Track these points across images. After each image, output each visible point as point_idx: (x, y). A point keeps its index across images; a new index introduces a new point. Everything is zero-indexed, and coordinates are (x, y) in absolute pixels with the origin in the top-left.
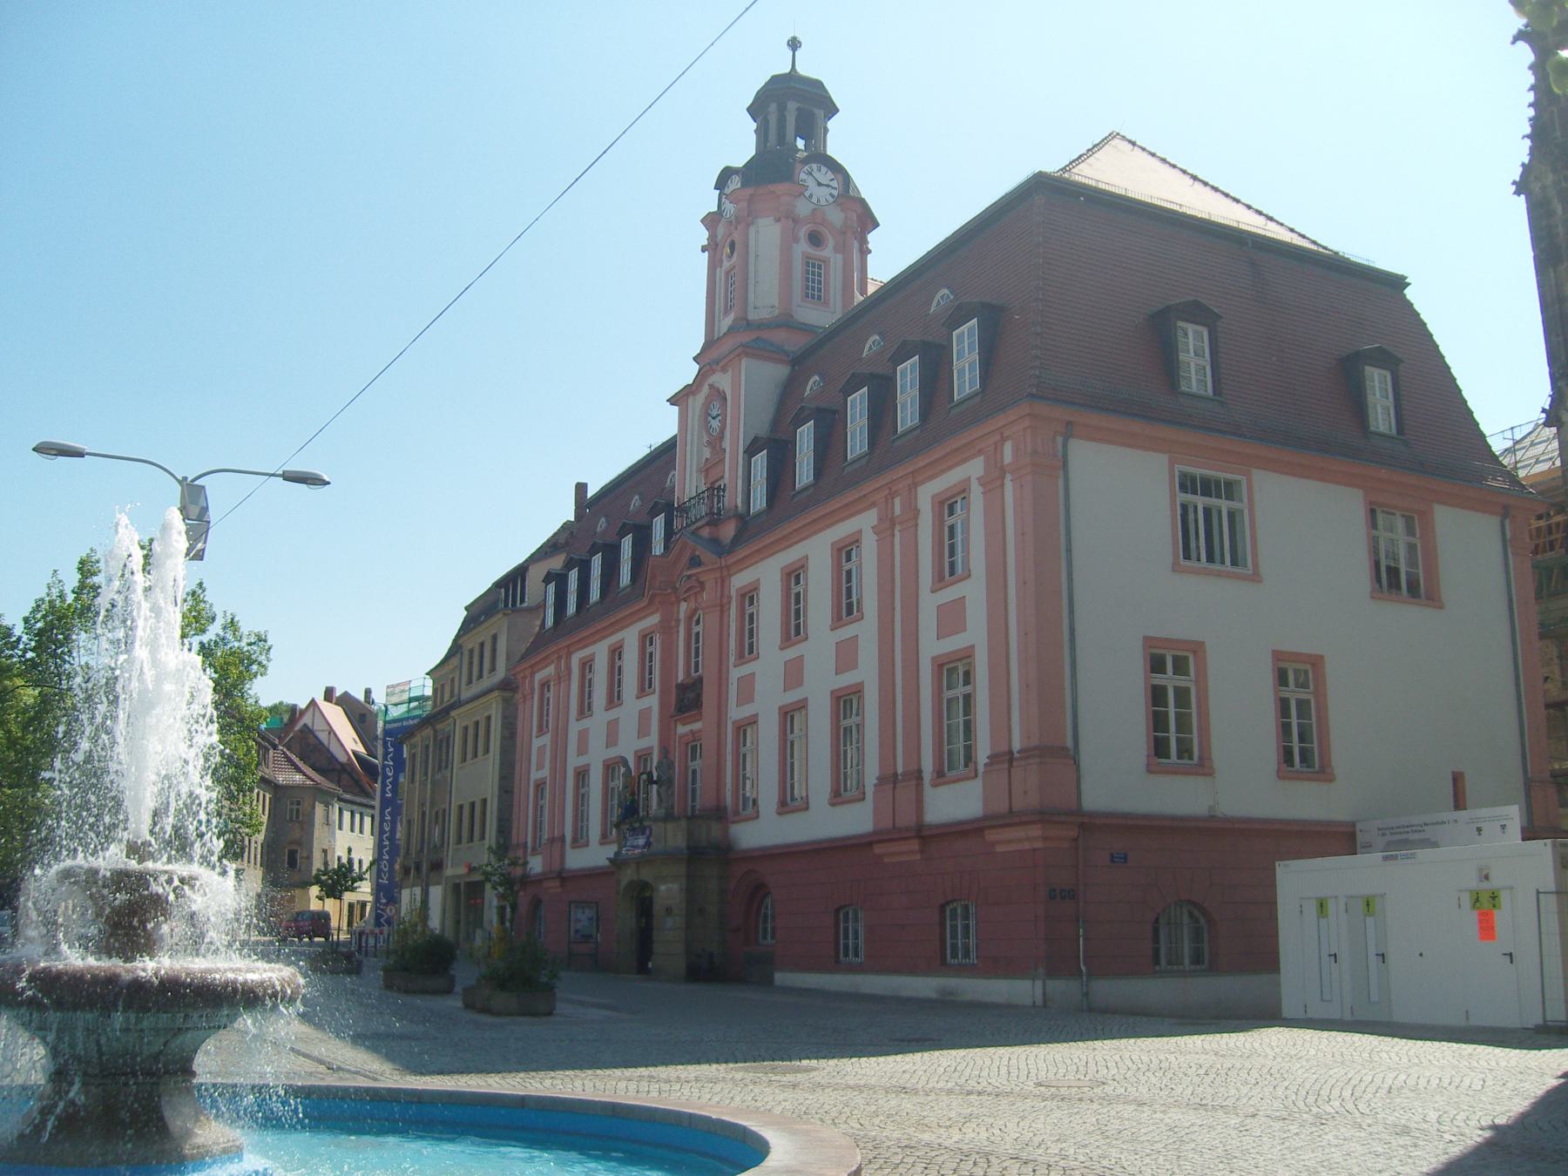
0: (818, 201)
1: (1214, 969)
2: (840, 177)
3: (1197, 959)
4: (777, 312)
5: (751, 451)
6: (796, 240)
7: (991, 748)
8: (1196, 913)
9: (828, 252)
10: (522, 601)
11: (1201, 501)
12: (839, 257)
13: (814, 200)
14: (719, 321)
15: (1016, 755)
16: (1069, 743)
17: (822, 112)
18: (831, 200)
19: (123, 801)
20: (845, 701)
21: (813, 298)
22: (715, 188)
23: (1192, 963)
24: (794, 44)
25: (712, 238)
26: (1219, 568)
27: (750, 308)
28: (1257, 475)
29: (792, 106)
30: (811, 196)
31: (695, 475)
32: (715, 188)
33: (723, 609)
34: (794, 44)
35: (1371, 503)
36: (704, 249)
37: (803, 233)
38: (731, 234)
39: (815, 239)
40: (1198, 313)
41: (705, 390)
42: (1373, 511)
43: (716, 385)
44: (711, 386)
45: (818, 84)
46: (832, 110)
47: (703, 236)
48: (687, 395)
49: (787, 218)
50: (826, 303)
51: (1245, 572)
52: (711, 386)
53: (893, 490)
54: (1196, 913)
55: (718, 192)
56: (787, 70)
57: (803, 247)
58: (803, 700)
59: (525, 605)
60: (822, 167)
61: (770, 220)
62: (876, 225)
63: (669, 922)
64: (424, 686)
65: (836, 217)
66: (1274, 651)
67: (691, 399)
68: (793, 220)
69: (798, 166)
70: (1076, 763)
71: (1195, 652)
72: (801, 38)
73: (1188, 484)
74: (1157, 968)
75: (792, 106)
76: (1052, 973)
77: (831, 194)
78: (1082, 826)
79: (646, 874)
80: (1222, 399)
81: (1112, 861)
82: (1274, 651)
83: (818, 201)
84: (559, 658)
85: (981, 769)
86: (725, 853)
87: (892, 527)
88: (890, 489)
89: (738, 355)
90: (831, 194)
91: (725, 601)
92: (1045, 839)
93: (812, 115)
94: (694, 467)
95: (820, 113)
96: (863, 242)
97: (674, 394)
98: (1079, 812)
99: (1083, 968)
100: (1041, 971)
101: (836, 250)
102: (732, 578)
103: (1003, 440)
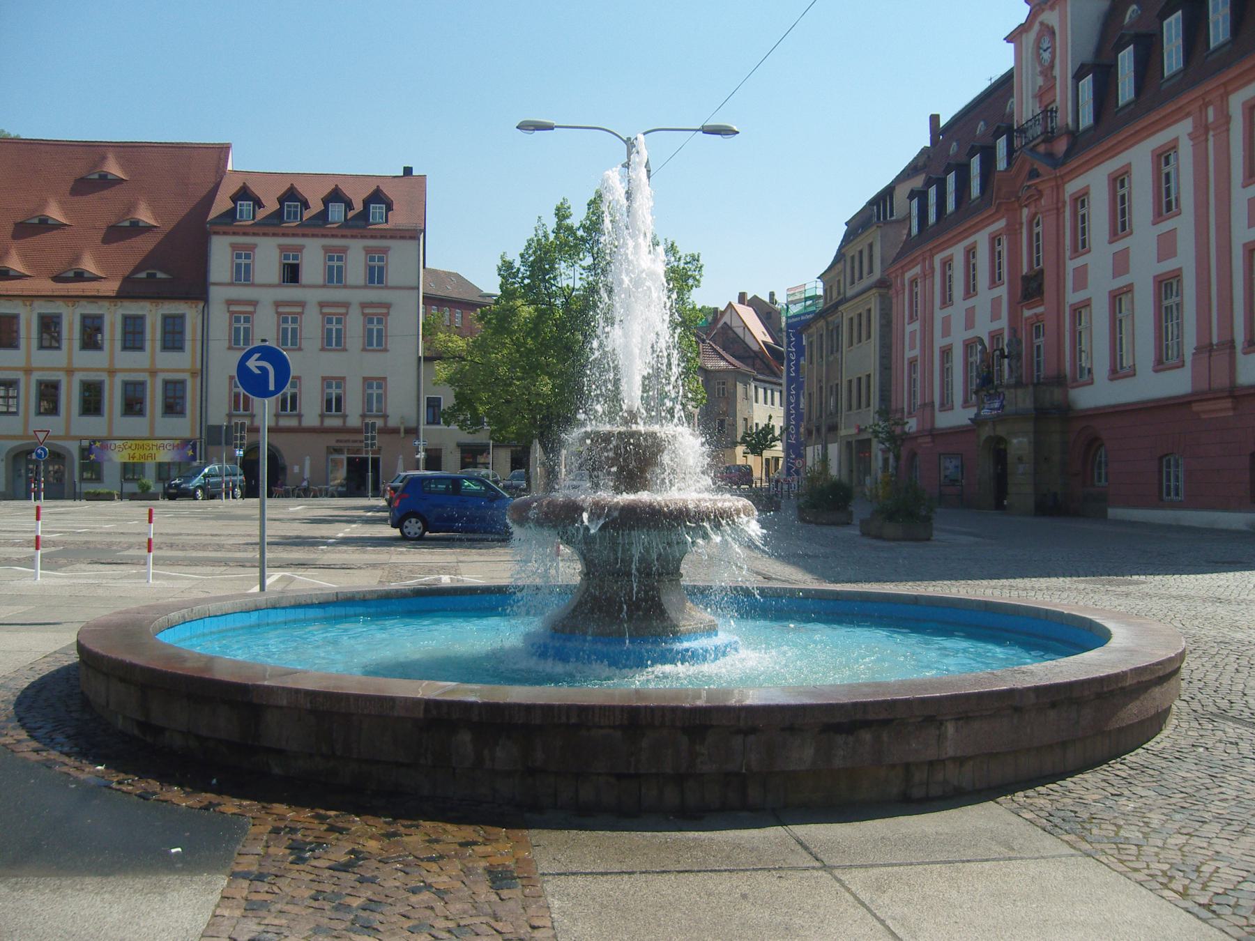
5: (1078, 76)
10: (892, 215)
33: (1059, 211)
41: (1036, 27)
52: (1042, 24)
59: (894, 218)
84: (924, 260)
86: (1066, 412)
87: (1207, 132)
88: (1204, 99)
94: (1030, 93)
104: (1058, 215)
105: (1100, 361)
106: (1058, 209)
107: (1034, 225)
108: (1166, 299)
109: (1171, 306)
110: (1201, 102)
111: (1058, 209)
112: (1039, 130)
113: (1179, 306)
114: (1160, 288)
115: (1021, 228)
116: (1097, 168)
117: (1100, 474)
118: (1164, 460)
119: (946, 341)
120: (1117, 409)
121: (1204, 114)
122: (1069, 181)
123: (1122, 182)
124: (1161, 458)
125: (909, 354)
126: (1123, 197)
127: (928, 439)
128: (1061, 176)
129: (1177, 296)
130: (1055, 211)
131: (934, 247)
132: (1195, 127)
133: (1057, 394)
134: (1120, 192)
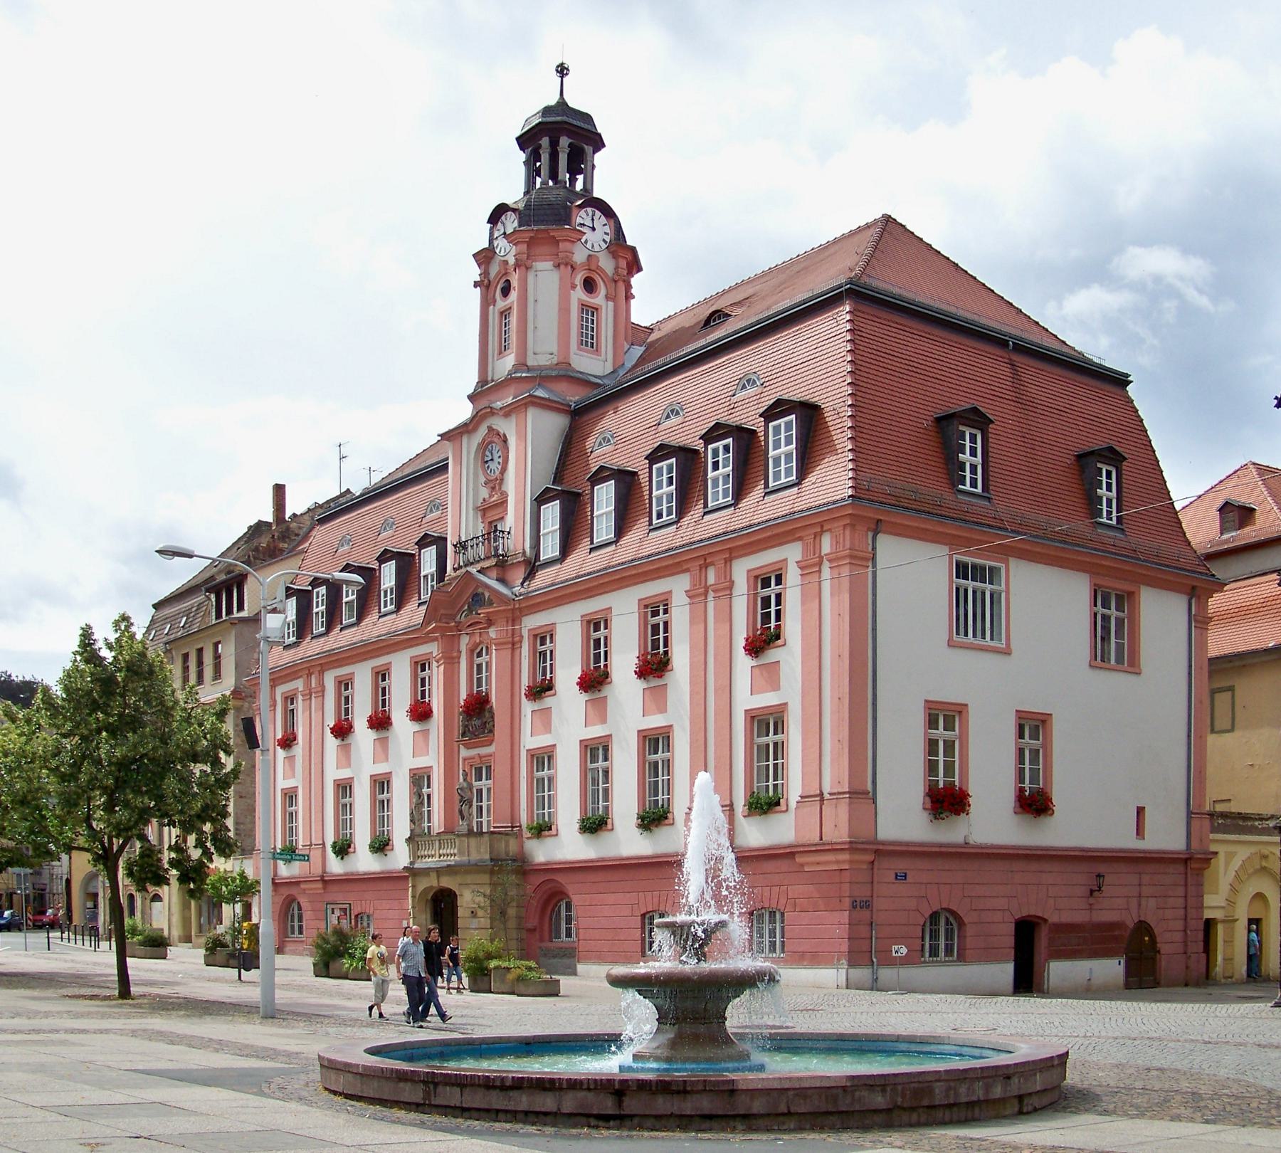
0: (593, 246)
1: (962, 958)
2: (612, 221)
3: (949, 950)
4: (555, 361)
5: (542, 499)
6: (574, 287)
7: (803, 789)
8: (951, 919)
9: (599, 299)
10: (241, 608)
11: (970, 585)
12: (611, 304)
13: (589, 246)
14: (493, 361)
15: (826, 796)
16: (869, 787)
17: (591, 149)
18: (604, 246)
19: (689, 880)
20: (382, 675)
21: (587, 345)
22: (488, 222)
23: (946, 956)
24: (562, 70)
25: (485, 274)
26: (980, 643)
27: (530, 353)
28: (1013, 562)
29: (564, 142)
30: (586, 241)
31: (471, 512)
32: (488, 222)
33: (514, 645)
34: (562, 70)
35: (1095, 585)
36: (476, 284)
37: (579, 280)
38: (506, 274)
39: (589, 285)
40: (978, 419)
41: (483, 431)
42: (1095, 591)
43: (494, 427)
44: (490, 429)
45: (587, 118)
46: (598, 143)
47: (475, 272)
48: (461, 434)
49: (566, 264)
50: (598, 351)
51: (1000, 645)
52: (490, 429)
53: (707, 561)
54: (951, 919)
55: (489, 225)
56: (553, 100)
57: (579, 294)
58: (351, 674)
59: (244, 614)
60: (597, 211)
61: (548, 265)
62: (639, 269)
63: (474, 923)
64: (1140, 885)
65: (607, 264)
66: (1017, 711)
67: (465, 439)
68: (572, 267)
69: (575, 211)
70: (874, 802)
71: (960, 712)
72: (568, 63)
73: (962, 570)
74: (923, 959)
75: (564, 142)
76: (852, 964)
77: (604, 240)
78: (877, 852)
79: (447, 882)
80: (989, 496)
81: (896, 878)
82: (1017, 711)
83: (593, 246)
84: (310, 675)
85: (793, 804)
86: (523, 867)
87: (706, 594)
88: (705, 560)
89: (525, 404)
90: (604, 240)
91: (517, 639)
92: (851, 862)
93: (582, 150)
94: (471, 506)
95: (588, 149)
96: (628, 287)
97: (447, 430)
98: (875, 842)
99: (874, 960)
100: (844, 961)
101: (607, 298)
102: (524, 619)
103: (822, 532)
104: (513, 649)
105: (568, 811)
106: (513, 644)
107: (475, 655)
108: (537, 771)
109: (543, 779)
110: (702, 562)
111: (513, 644)
112: (481, 550)
113: (668, 763)
114: (532, 763)
115: (459, 657)
116: (583, 601)
117: (293, 927)
118: (647, 916)
119: (344, 774)
120: (943, 849)
121: (703, 575)
122: (526, 615)
123: (347, 685)
124: (643, 916)
125: (282, 783)
126: (384, 689)
127: (320, 885)
128: (520, 609)
129: (549, 769)
130: (510, 646)
131: (327, 663)
132: (693, 585)
133: (513, 846)
134: (345, 693)
